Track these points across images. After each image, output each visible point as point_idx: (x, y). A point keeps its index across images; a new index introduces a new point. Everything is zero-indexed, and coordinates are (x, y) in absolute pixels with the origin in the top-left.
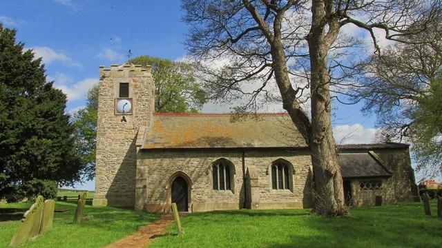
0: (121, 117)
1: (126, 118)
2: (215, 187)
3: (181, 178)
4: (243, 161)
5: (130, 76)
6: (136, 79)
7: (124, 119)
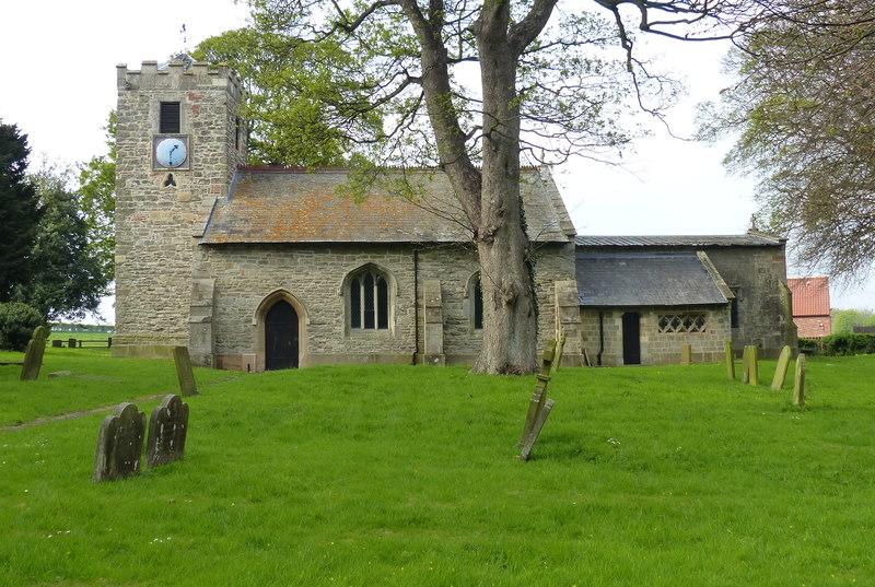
0: (165, 178)
1: (175, 178)
2: (356, 324)
3: (283, 301)
4: (601, 318)
5: (183, 87)
6: (196, 92)
7: (170, 181)
